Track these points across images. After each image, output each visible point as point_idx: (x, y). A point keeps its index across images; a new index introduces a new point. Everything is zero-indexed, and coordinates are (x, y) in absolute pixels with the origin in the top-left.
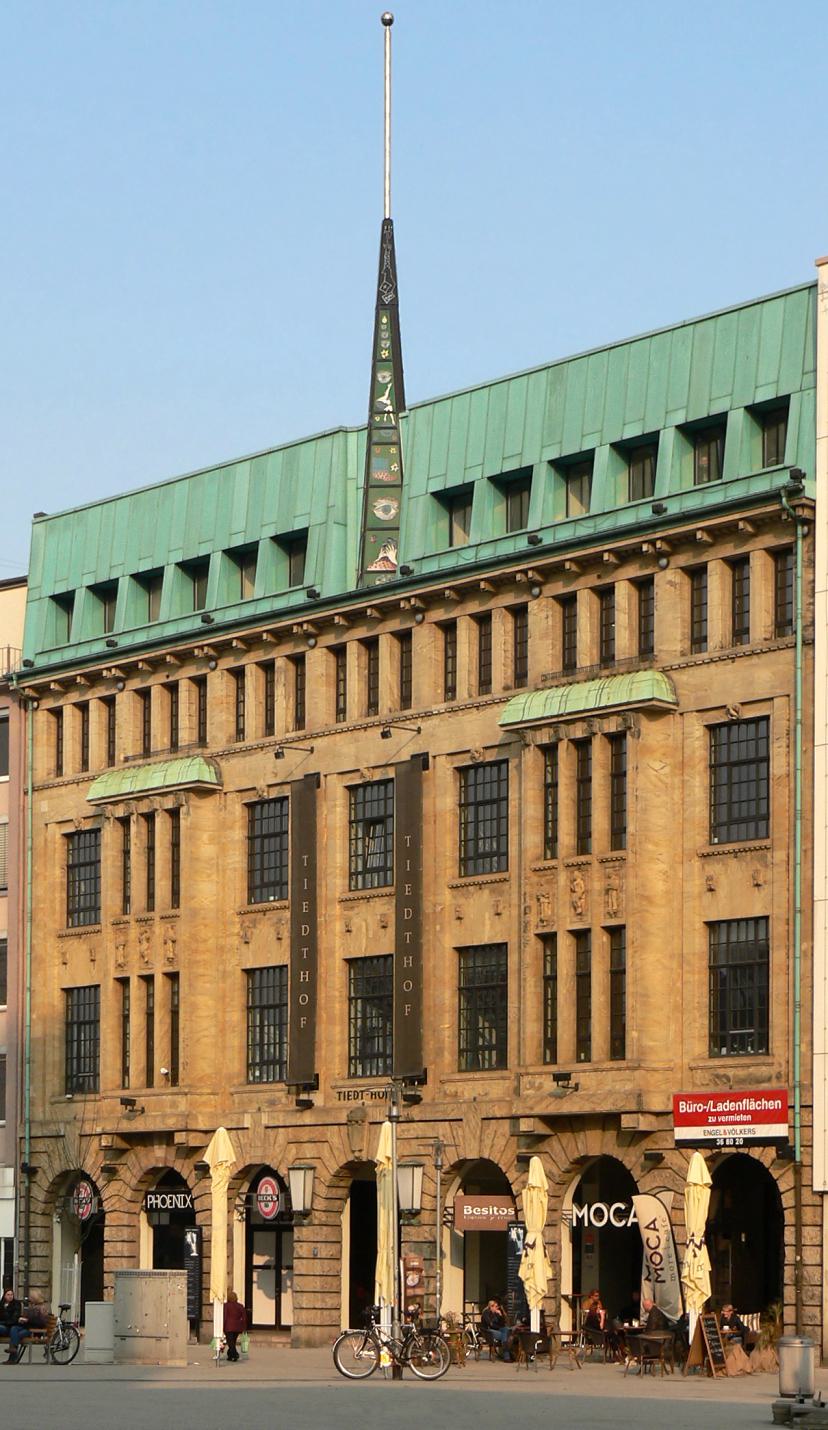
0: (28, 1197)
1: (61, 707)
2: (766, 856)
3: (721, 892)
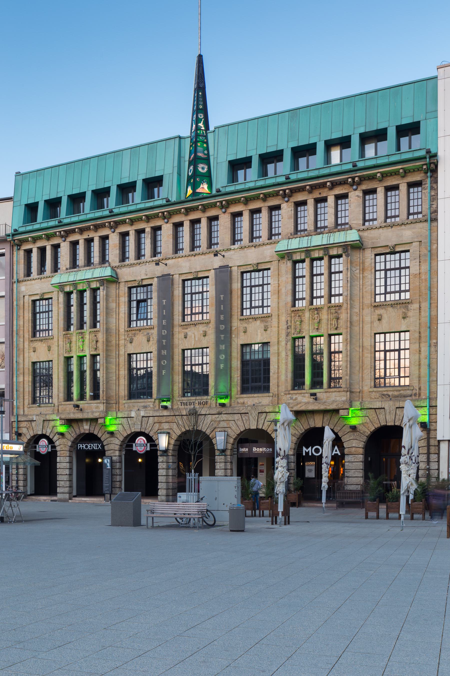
2: (408, 307)
3: (384, 321)
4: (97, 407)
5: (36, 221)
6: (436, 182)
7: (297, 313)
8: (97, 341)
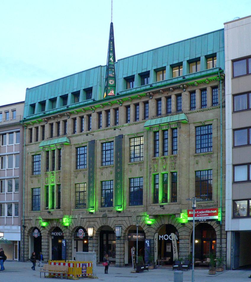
0: (24, 233)
1: (32, 128)
3: (200, 164)
4: (59, 213)
5: (34, 114)
6: (224, 86)
7: (155, 161)
8: (59, 177)
